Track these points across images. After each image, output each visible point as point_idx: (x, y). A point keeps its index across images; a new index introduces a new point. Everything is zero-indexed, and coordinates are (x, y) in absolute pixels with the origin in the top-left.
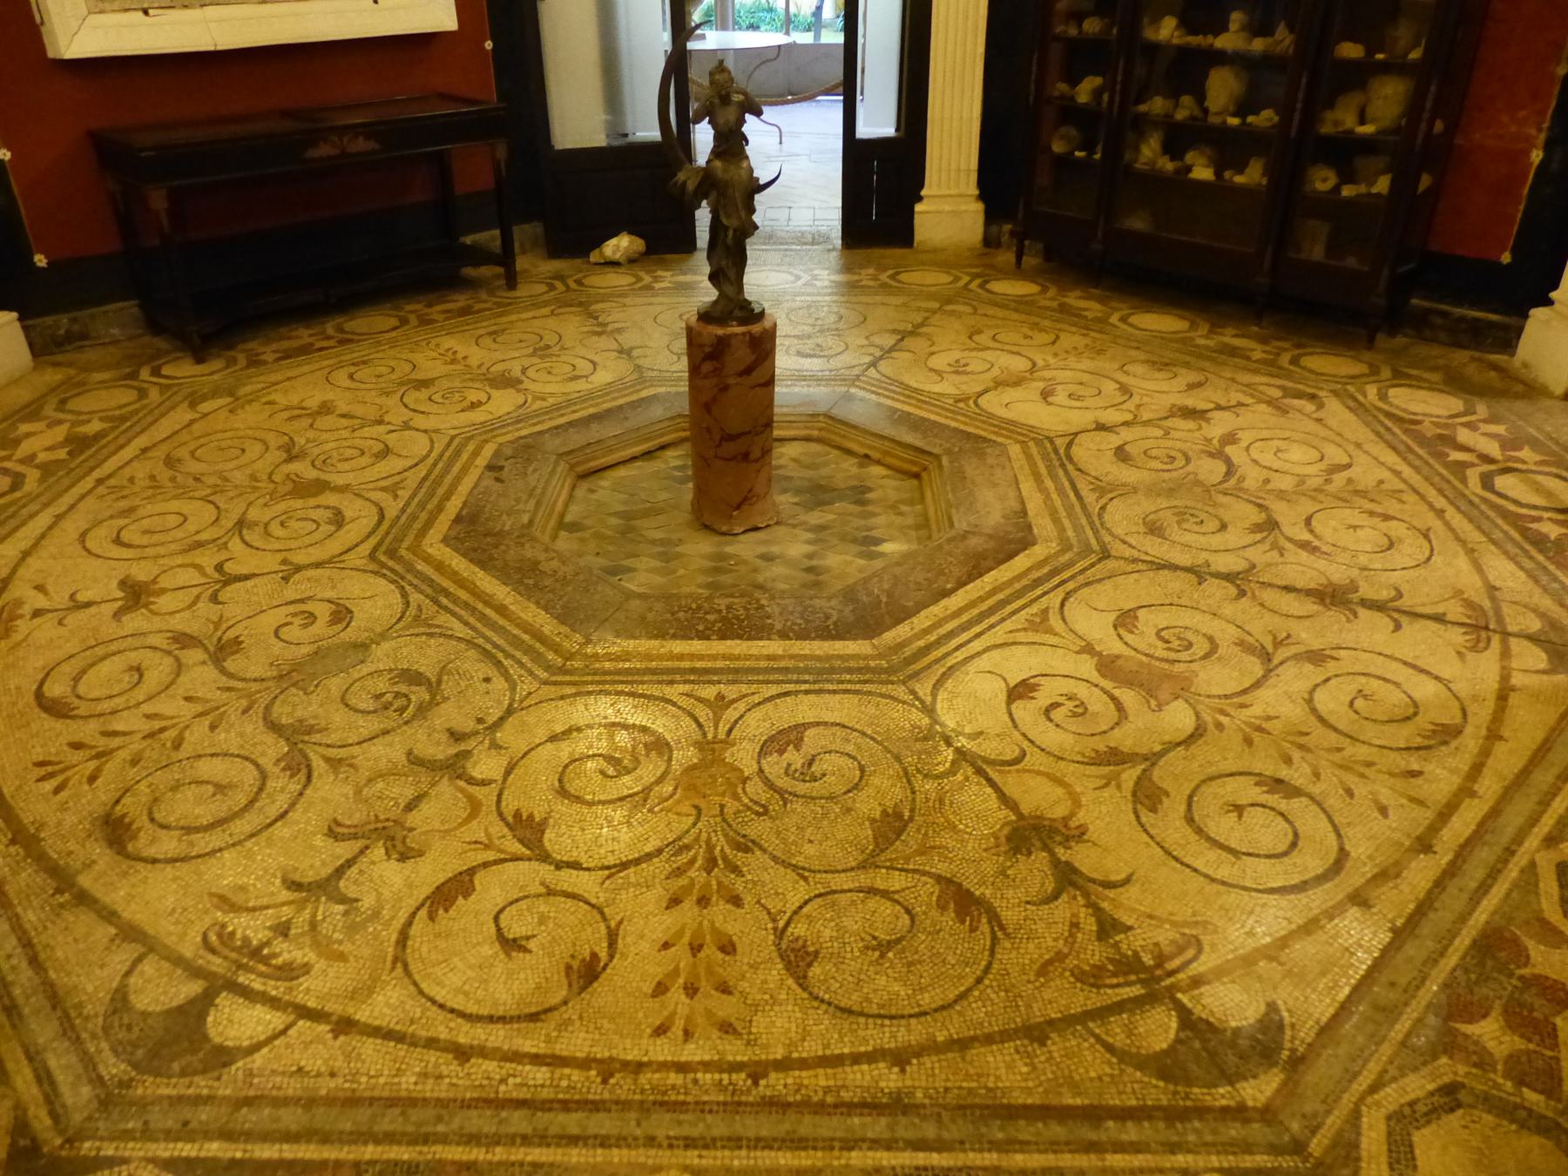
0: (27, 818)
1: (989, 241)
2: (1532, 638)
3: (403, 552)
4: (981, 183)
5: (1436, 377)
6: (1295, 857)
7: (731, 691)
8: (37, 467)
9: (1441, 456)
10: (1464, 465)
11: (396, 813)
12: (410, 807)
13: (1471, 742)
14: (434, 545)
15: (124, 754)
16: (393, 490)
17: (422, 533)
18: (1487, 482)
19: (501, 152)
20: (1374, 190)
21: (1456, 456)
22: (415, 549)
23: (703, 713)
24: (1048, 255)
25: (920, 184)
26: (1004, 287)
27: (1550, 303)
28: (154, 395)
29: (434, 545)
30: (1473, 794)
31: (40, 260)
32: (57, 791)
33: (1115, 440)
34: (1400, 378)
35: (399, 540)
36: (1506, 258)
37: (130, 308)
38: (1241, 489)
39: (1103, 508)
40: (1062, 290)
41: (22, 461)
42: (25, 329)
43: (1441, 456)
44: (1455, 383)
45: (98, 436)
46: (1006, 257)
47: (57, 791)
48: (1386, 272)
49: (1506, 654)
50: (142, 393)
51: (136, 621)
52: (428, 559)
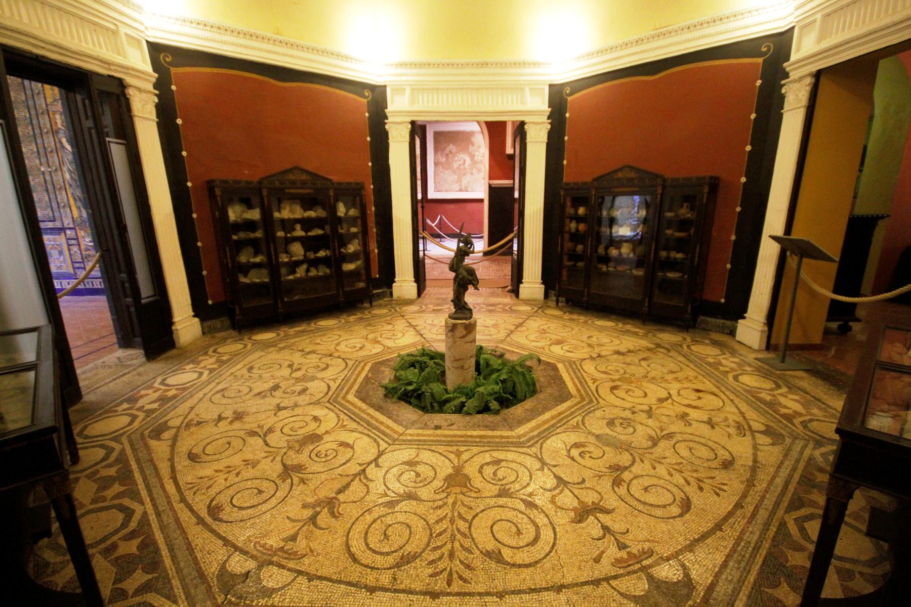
1: (546, 296)
2: (761, 432)
3: (340, 399)
4: (542, 279)
5: (707, 341)
7: (463, 449)
8: (144, 412)
9: (717, 369)
10: (727, 372)
13: (691, 444)
14: (351, 397)
16: (334, 380)
17: (347, 392)
18: (736, 378)
19: (78, 591)
20: (298, 275)
21: (722, 368)
22: (344, 398)
23: (452, 456)
24: (567, 302)
25: (394, 277)
26: (549, 312)
27: (744, 318)
28: (249, 346)
29: (351, 397)
31: (210, 302)
34: (696, 342)
35: (338, 396)
36: (723, 301)
37: (142, 351)
38: (806, 440)
39: (597, 387)
40: (571, 313)
41: (137, 409)
42: (202, 325)
43: (717, 369)
44: (715, 343)
45: (174, 397)
46: (553, 304)
48: (690, 306)
49: (754, 438)
50: (245, 346)
52: (348, 401)
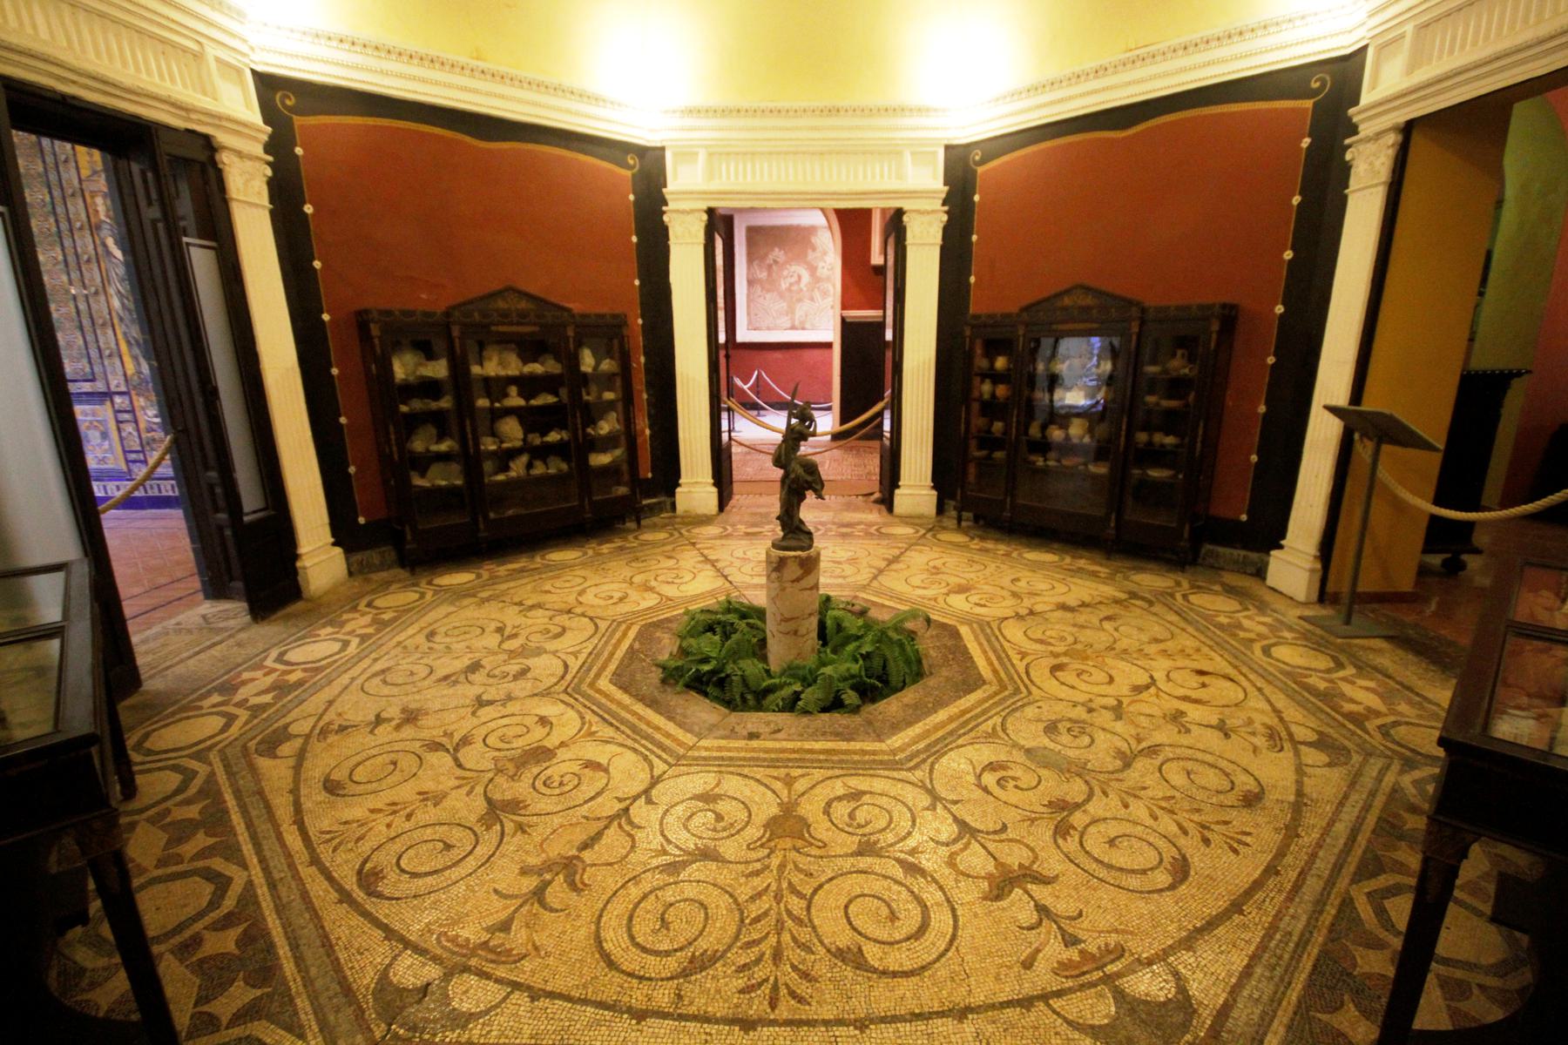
0: (1279, 837)
1: (940, 509)
2: (1310, 744)
3: (584, 687)
4: (933, 480)
5: (1217, 588)
6: (843, 901)
7: (796, 772)
9: (1234, 635)
10: (1252, 641)
11: (574, 852)
12: (585, 846)
14: (604, 683)
15: (1196, 817)
16: (575, 655)
17: (598, 675)
18: (1266, 651)
21: (1242, 634)
22: (592, 685)
23: (778, 785)
24: (976, 519)
26: (944, 536)
27: (1281, 547)
28: (429, 596)
29: (604, 683)
30: (311, 864)
31: (362, 520)
32: (1249, 834)
33: (1162, 646)
34: (1198, 589)
35: (581, 681)
36: (1244, 517)
39: (1027, 666)
40: (982, 539)
42: (347, 559)
43: (1234, 635)
44: (1231, 591)
46: (952, 523)
47: (1249, 834)
48: (1187, 527)
49: (1297, 754)
50: (422, 595)
51: (408, 732)
52: (599, 691)
